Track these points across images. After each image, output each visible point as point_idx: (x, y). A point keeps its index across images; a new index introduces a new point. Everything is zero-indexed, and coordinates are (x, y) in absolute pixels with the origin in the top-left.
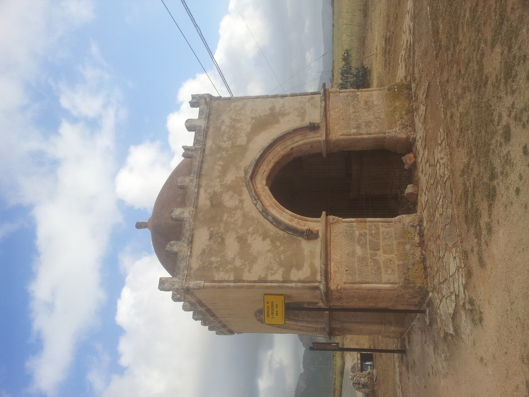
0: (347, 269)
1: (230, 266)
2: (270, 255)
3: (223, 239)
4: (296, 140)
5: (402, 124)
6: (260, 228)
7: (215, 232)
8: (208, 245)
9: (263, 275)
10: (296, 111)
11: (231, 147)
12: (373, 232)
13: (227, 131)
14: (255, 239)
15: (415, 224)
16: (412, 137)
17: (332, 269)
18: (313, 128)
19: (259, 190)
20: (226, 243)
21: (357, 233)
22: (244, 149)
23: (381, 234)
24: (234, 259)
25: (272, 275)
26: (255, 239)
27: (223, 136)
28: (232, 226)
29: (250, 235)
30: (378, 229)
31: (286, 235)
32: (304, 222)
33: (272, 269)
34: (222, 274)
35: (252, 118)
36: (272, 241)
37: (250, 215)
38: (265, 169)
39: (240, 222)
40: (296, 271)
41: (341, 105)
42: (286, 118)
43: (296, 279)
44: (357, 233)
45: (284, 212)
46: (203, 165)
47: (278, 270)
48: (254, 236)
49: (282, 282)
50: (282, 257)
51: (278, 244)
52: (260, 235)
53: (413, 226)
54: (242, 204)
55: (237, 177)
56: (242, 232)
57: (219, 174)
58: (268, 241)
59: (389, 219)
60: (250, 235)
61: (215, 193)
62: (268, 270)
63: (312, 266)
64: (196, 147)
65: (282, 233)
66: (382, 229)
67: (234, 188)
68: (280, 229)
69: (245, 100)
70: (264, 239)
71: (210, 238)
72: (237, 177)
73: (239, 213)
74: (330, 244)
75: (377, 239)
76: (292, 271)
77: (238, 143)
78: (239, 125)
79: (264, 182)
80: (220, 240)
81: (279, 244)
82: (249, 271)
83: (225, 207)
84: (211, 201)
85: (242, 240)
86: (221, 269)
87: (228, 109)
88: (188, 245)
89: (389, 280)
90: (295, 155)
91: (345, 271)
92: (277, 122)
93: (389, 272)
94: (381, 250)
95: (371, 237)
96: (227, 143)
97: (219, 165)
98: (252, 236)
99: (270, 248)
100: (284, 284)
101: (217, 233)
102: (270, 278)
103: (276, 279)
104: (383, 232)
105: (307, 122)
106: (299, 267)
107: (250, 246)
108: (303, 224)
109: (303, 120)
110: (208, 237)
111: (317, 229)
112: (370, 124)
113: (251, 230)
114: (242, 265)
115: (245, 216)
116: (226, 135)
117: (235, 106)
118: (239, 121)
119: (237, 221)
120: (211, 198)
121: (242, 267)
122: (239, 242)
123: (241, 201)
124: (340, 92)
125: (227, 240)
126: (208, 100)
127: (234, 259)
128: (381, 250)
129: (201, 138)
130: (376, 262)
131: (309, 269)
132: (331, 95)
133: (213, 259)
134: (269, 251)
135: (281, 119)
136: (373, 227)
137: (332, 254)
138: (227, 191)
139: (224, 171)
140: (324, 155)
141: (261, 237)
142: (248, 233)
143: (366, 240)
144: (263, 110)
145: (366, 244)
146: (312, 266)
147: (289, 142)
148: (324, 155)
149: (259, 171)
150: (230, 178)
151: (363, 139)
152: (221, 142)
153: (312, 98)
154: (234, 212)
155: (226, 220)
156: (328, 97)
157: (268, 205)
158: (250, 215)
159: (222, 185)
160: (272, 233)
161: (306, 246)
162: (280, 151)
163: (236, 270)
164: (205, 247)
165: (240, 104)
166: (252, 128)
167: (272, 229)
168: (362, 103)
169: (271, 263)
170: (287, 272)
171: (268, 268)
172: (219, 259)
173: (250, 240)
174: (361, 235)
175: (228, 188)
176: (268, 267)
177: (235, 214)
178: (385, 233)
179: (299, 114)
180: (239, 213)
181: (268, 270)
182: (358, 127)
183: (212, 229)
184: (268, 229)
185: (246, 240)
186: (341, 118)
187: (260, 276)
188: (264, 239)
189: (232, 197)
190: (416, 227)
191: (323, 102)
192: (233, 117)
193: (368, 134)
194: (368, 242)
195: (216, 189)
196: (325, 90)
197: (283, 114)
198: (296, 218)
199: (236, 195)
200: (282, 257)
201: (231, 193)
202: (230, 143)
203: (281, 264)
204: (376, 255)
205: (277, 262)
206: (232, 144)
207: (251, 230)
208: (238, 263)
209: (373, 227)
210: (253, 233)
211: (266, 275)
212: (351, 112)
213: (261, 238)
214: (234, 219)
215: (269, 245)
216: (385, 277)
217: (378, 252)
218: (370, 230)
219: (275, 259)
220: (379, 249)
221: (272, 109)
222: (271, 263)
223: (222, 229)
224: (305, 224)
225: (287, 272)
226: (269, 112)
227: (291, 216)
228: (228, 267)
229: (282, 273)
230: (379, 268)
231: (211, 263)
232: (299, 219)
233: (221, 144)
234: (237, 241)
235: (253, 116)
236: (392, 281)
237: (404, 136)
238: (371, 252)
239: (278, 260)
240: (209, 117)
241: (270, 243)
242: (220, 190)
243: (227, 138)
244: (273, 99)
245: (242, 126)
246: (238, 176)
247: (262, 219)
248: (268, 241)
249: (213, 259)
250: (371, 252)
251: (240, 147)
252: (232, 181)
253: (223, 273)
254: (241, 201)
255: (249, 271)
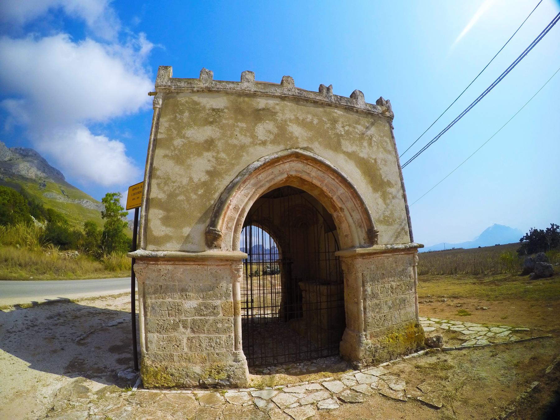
0: (163, 287)
1: (175, 132)
2: (185, 181)
3: (211, 123)
4: (353, 214)
5: (376, 348)
6: (224, 167)
7: (221, 114)
8: (205, 107)
9: (158, 173)
10: (389, 212)
11: (337, 134)
12: (220, 325)
13: (357, 130)
14: (209, 161)
15: (231, 380)
16: (360, 365)
17: (164, 266)
18: (372, 236)
19: (282, 165)
20: (206, 127)
21: (218, 302)
22: (336, 147)
23: (217, 335)
24: (184, 137)
25: (158, 184)
26: (209, 161)
27: (349, 125)
28: (229, 133)
29: (215, 154)
30: (225, 331)
31: (212, 202)
32: (234, 227)
33: (166, 184)
34: (166, 125)
35: (375, 160)
36: (204, 184)
37: (244, 154)
38: (313, 175)
39: (235, 142)
40: (160, 216)
41: (400, 270)
42: (380, 201)
43: (150, 216)
44: (218, 302)
45: (249, 200)
46: (311, 102)
47: (164, 192)
48: (213, 160)
49: (148, 199)
50: (181, 198)
51: (201, 192)
52: (215, 168)
53: (229, 376)
54: (260, 144)
55: (297, 138)
56: (220, 144)
57: (301, 118)
58: (205, 178)
59: (240, 346)
60: (215, 154)
61: (275, 113)
62: (164, 179)
63: (167, 239)
64: (333, 97)
65: (216, 196)
66: (224, 337)
67: (282, 135)
68: (222, 193)
69: (394, 153)
70: (208, 172)
71: (213, 110)
72: (297, 138)
73: (247, 140)
74: (199, 265)
75: (209, 330)
76: (161, 211)
77: (343, 142)
78: (365, 144)
79: (293, 173)
80: (211, 120)
81: (199, 193)
82: (166, 156)
83: (256, 124)
84: (263, 109)
85: (209, 144)
86: (173, 123)
87: (382, 135)
88: (207, 88)
89: (151, 342)
90: (335, 215)
91: (160, 284)
92: (375, 190)
93: (161, 343)
94: (192, 335)
95: (211, 321)
96: (341, 129)
97: (312, 120)
98: (213, 157)
99: (196, 180)
100: (145, 201)
101: (220, 116)
102: (154, 182)
103: (152, 190)
104: (220, 338)
105: (377, 227)
106: (166, 221)
107: (199, 155)
108: (229, 225)
109: (380, 222)
110: (214, 107)
111: (223, 245)
112: (377, 310)
113: (223, 155)
114: (174, 147)
115: (243, 147)
116: (351, 129)
117: (386, 142)
118: (370, 144)
119: (236, 139)
120: (268, 109)
121: (172, 148)
122: (206, 141)
123: (264, 143)
124: (414, 267)
125: (210, 127)
126: (387, 114)
127: (184, 137)
128: (192, 335)
129: (343, 103)
130: (175, 327)
131: (162, 234)
132: (411, 256)
133: (186, 114)
134: (191, 179)
135: (378, 194)
136: (226, 325)
137: (184, 267)
138: (277, 127)
139: (303, 124)
140: (338, 253)
141: (212, 169)
142: (218, 152)
143: (207, 315)
144: (387, 172)
145: (201, 315)
146: (167, 239)
147: (350, 205)
148: (338, 253)
149: (308, 166)
150: (296, 130)
151: (358, 303)
152: (342, 123)
153: (406, 233)
154: (248, 134)
155: (237, 126)
156: (408, 252)
157: (260, 177)
158: (244, 154)
159: (286, 121)
160: (217, 183)
161: (193, 230)
162: (338, 193)
163: (170, 139)
164: (202, 105)
165: (390, 147)
166: (363, 158)
167: (222, 184)
168: (403, 296)
169: (174, 182)
170: (160, 205)
171: (167, 180)
172: (185, 120)
173: (208, 155)
174: (215, 307)
175: (282, 128)
176: (169, 178)
177: (245, 135)
178: (218, 340)
179: (387, 216)
180: (247, 140)
181: (164, 179)
182: (374, 296)
183: (226, 110)
184: (223, 178)
185: (208, 150)
186: (384, 272)
187: (157, 170)
188: (208, 172)
189: (270, 132)
190: (228, 380)
191: (403, 246)
192: (374, 139)
193: (365, 308)
194: (203, 318)
195: (279, 114)
196: (416, 248)
197: (384, 196)
198: (240, 215)
199: (272, 137)
200: (181, 198)
201: (276, 131)
202: (343, 133)
203: (172, 196)
204: (185, 327)
205: (175, 190)
206: (342, 135)
207: (223, 155)
208: (178, 142)
209: (226, 325)
210: (217, 159)
211: (158, 177)
212: (392, 283)
213: (209, 168)
214: (239, 135)
215: (200, 180)
216: (154, 336)
217: (189, 330)
218: (222, 321)
219: (179, 187)
220: (193, 332)
221: (389, 184)
222: (174, 182)
223: (224, 121)
224: (230, 228)
225: (160, 205)
226: (385, 180)
227: (243, 210)
228: (174, 131)
229: (159, 197)
230: (167, 330)
231: (182, 112)
232: (239, 220)
233: (340, 123)
234: (207, 140)
235: (379, 161)
236: (149, 345)
237: (361, 355)
238: (189, 321)
239: (177, 192)
240: (369, 113)
241: (203, 180)
242: (279, 119)
243: (348, 130)
244: (400, 185)
245: (365, 147)
246: (299, 140)
247: (238, 169)
248: (205, 178)
249: (186, 114)
250: (189, 321)
251: (339, 144)
252: (292, 133)
253: (168, 126)
254: (264, 143)
255: (166, 156)
